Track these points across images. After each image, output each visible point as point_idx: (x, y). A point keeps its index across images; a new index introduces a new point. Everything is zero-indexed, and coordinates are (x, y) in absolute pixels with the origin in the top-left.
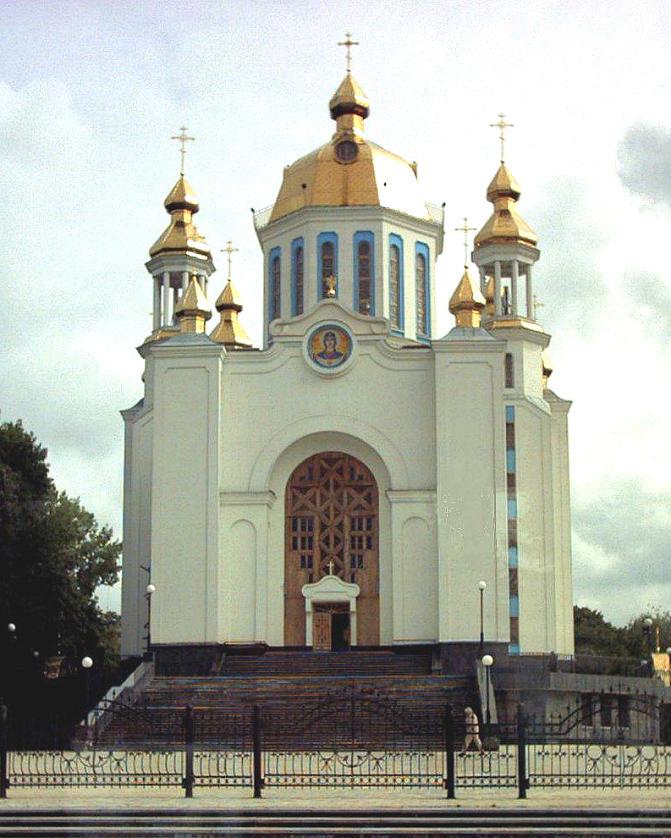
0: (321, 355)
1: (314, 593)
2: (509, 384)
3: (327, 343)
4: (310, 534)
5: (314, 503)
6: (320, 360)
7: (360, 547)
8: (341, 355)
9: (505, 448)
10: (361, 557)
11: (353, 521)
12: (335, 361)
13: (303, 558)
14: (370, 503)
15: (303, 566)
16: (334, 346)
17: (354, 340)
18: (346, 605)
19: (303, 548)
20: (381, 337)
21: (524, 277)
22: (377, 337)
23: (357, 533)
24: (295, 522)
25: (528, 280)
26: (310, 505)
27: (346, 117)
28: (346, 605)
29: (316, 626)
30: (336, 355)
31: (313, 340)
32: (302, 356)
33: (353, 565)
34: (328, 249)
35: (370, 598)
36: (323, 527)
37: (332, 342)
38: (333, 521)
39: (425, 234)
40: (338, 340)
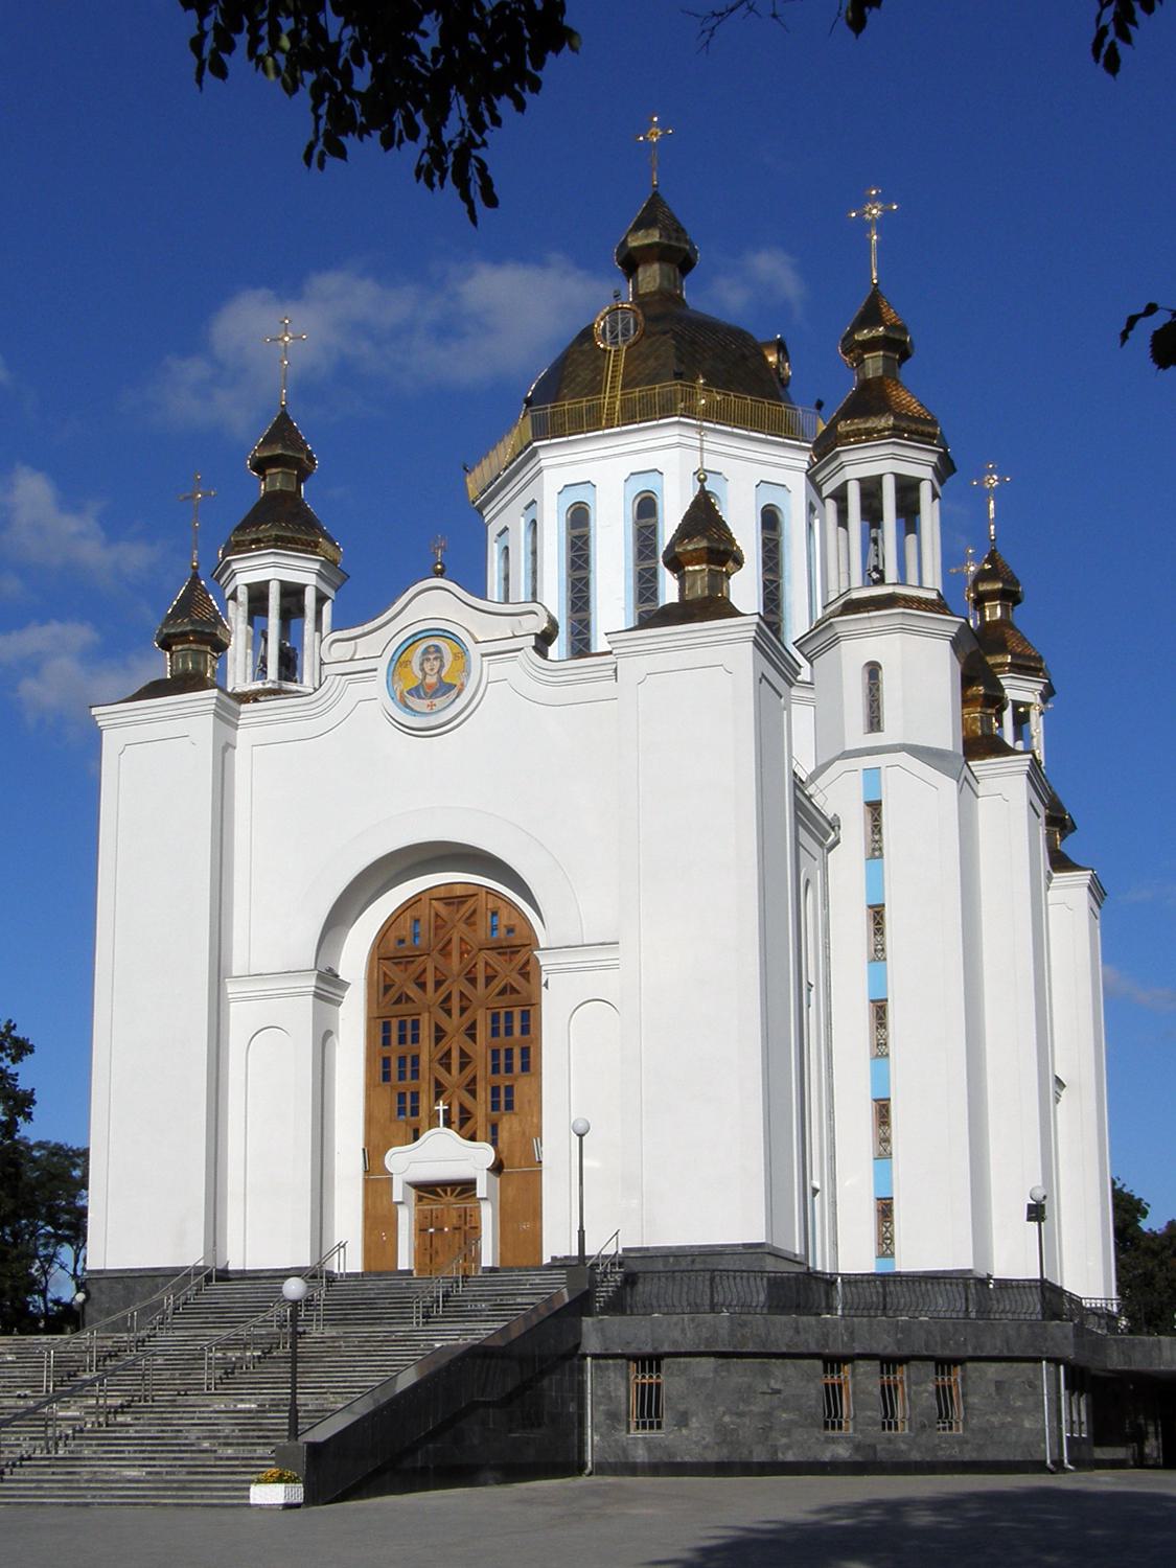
0: (415, 692)
3: (427, 666)
6: (413, 702)
7: (509, 1068)
8: (451, 687)
9: (883, 803)
10: (509, 1090)
12: (439, 702)
13: (402, 1096)
15: (402, 1111)
16: (439, 672)
17: (474, 651)
19: (402, 1077)
21: (421, 163)
23: (502, 1041)
24: (386, 1027)
25: (420, 160)
30: (444, 688)
31: (399, 662)
33: (495, 1106)
35: (518, 1172)
36: (440, 1034)
37: (437, 664)
38: (454, 1024)
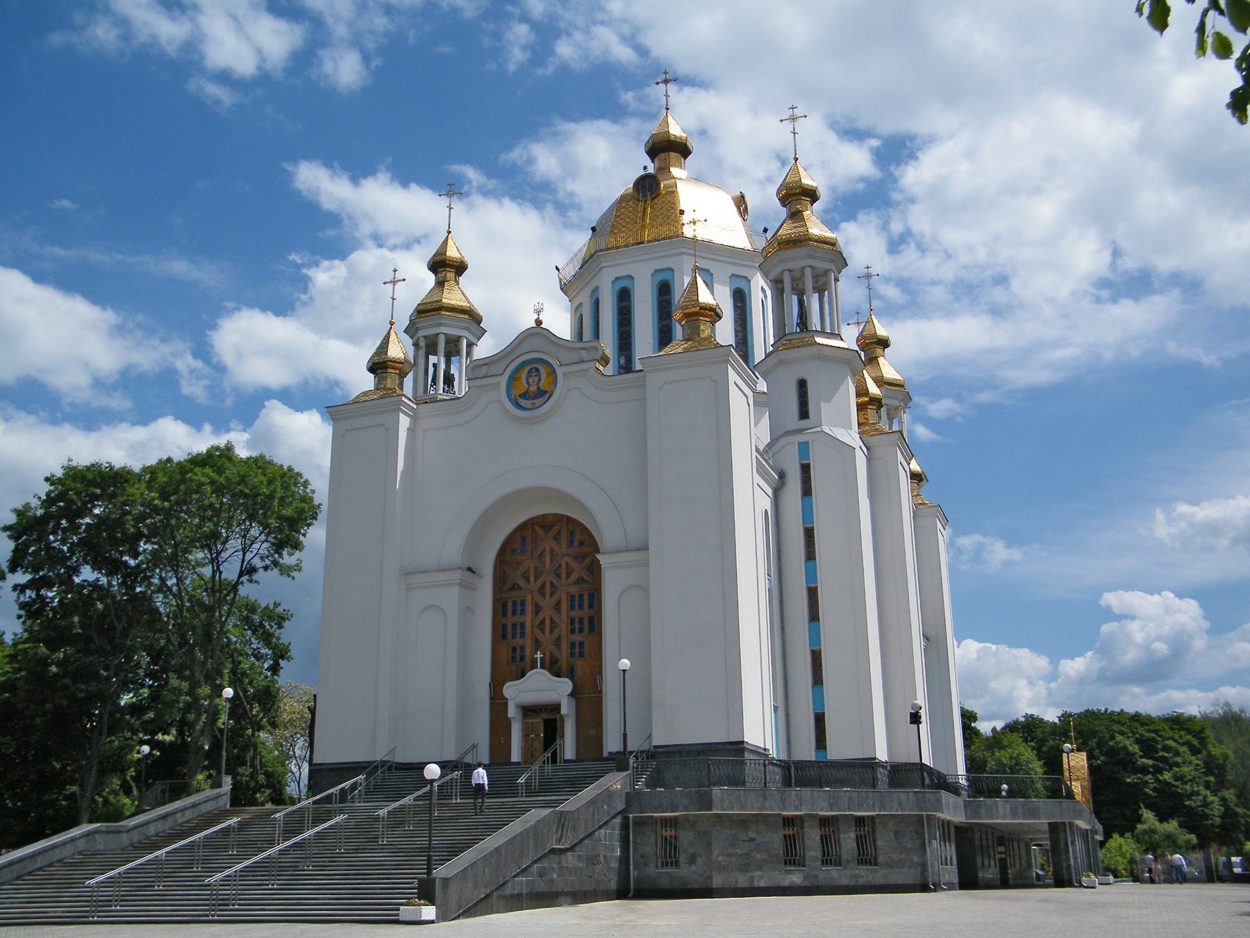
0: (524, 396)
1: (518, 692)
2: (804, 414)
3: (531, 380)
4: (573, 614)
5: (527, 579)
6: (523, 402)
8: (545, 392)
11: (572, 598)
14: (592, 573)
17: (560, 371)
18: (556, 708)
20: (591, 365)
22: (583, 366)
26: (521, 583)
27: (663, 155)
28: (556, 708)
29: (526, 735)
31: (513, 378)
32: (500, 401)
34: (624, 298)
38: (547, 602)
39: (743, 266)
40: (543, 375)
